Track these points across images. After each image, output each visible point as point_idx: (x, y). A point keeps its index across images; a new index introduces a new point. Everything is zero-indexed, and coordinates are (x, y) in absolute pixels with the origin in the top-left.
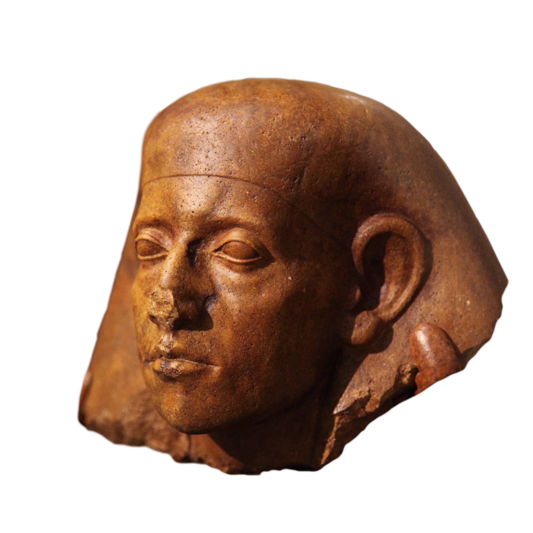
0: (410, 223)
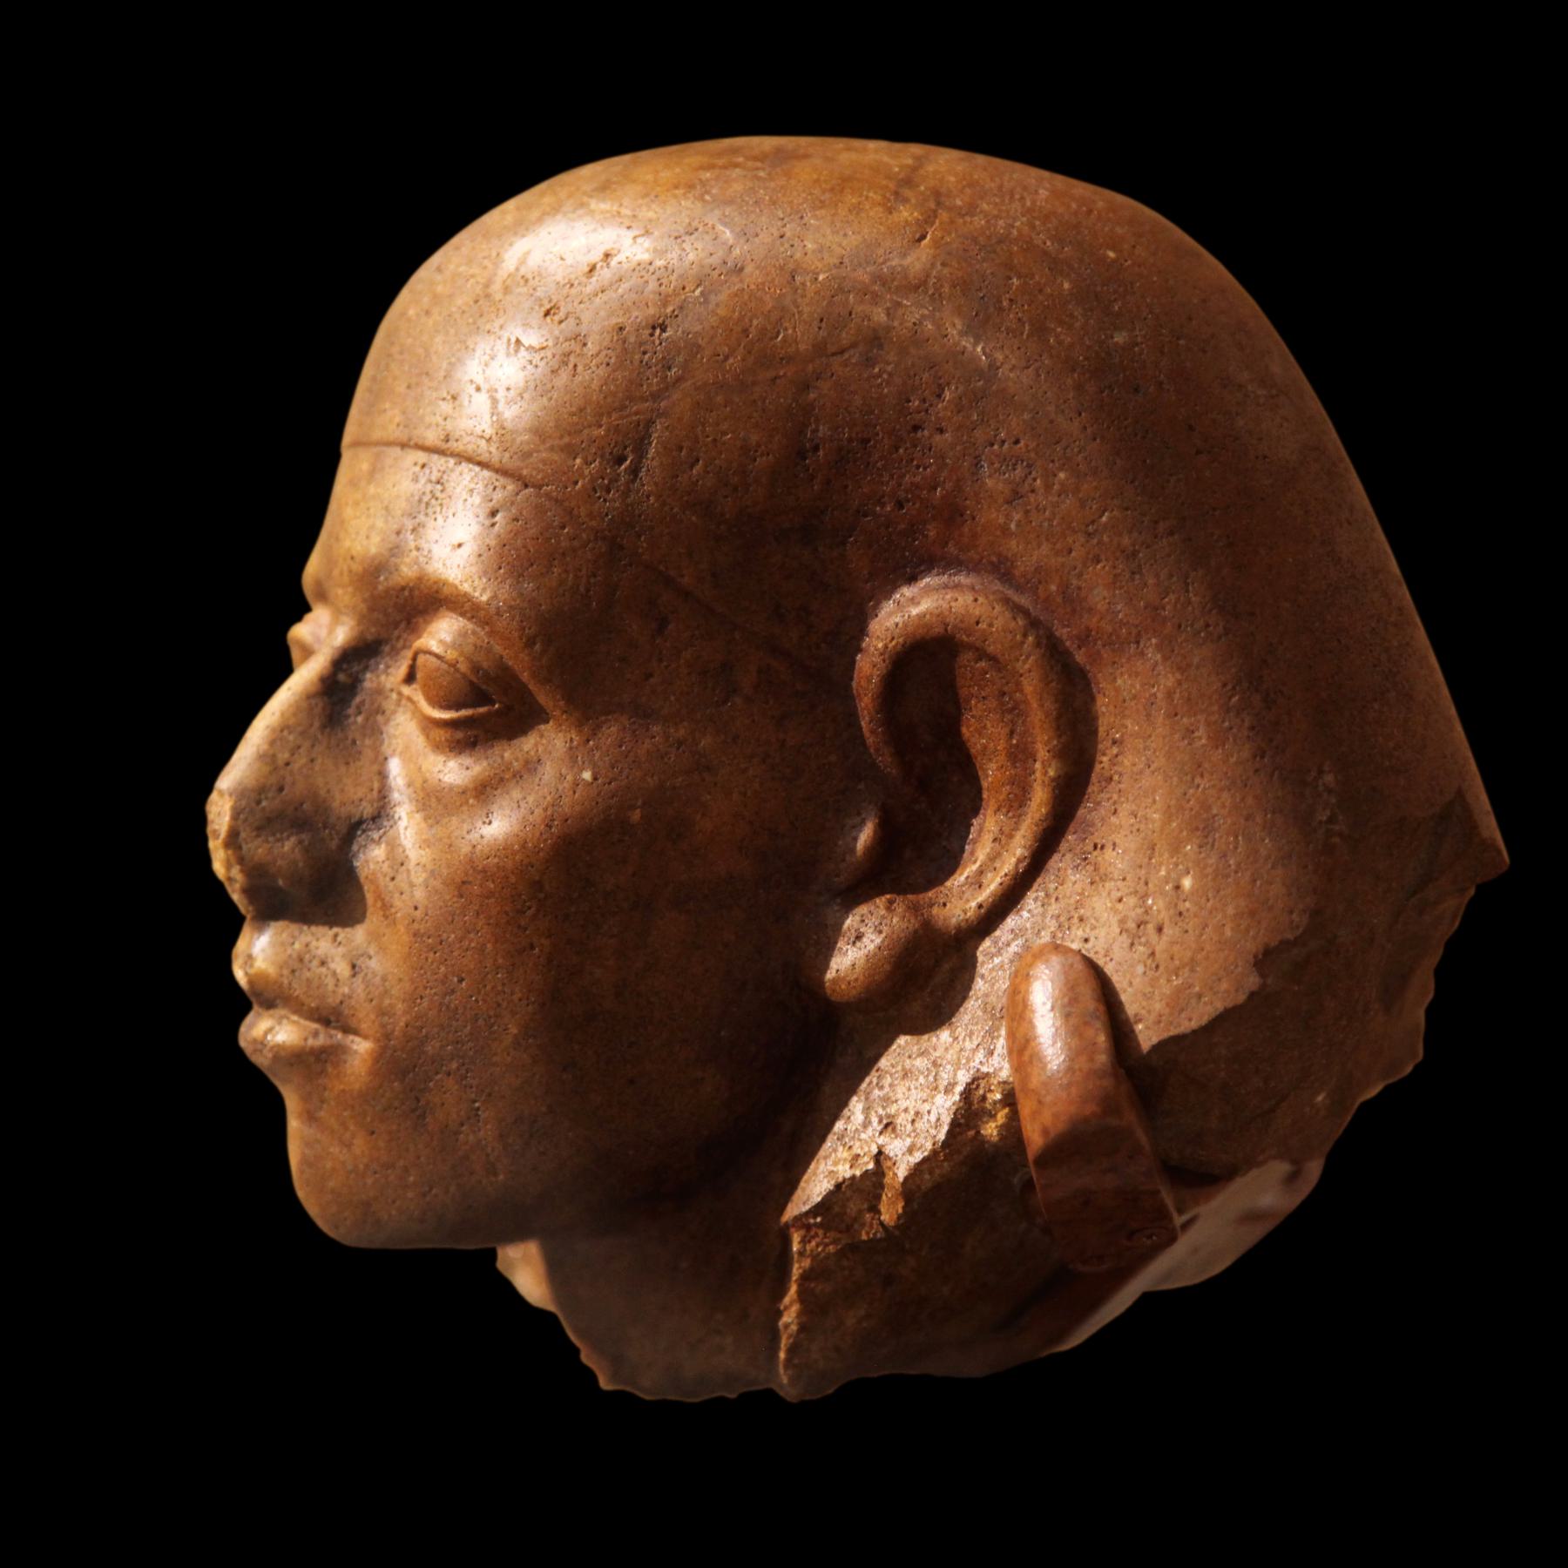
0: (1018, 610)
